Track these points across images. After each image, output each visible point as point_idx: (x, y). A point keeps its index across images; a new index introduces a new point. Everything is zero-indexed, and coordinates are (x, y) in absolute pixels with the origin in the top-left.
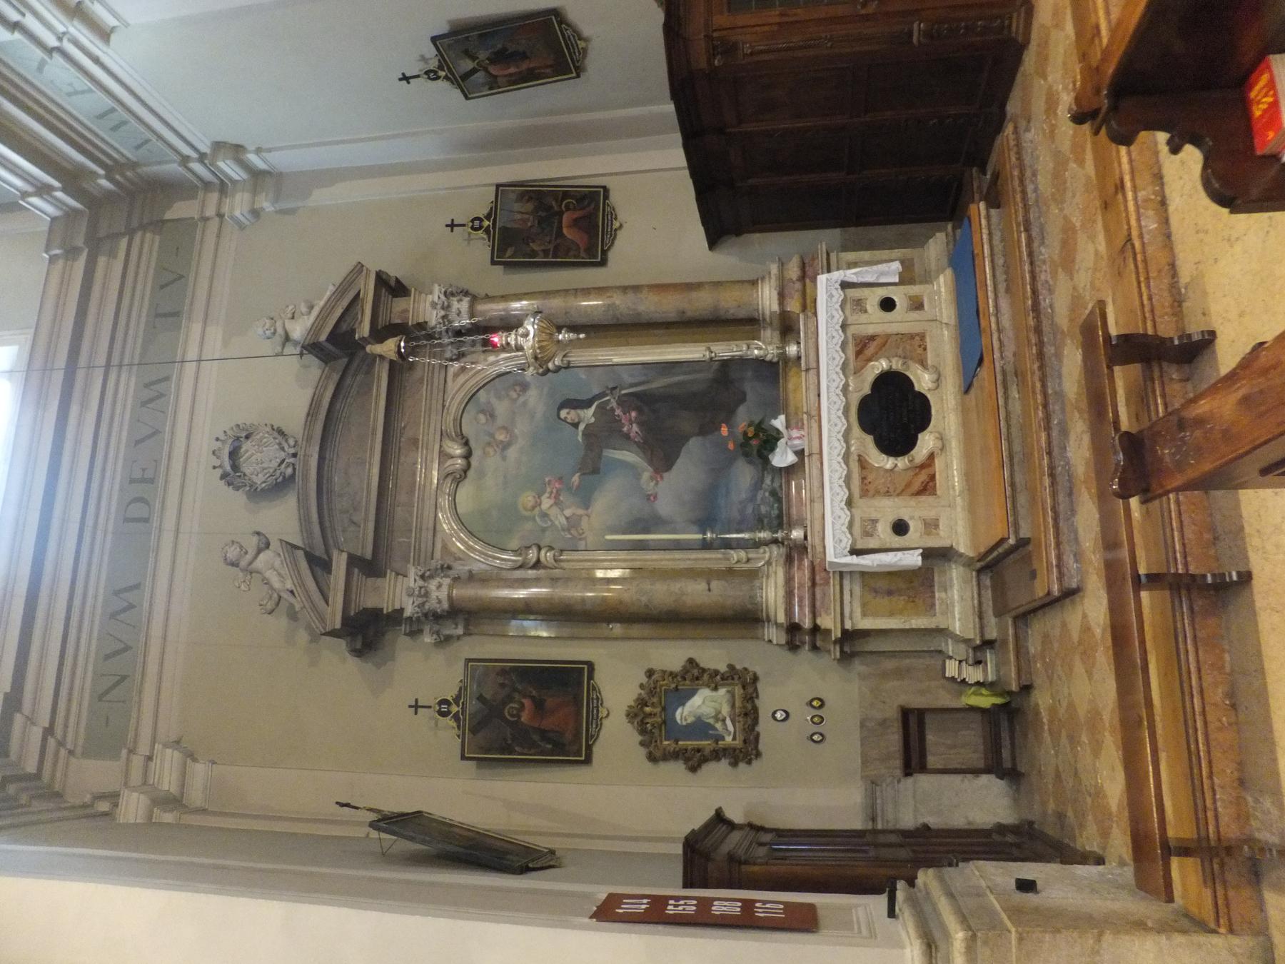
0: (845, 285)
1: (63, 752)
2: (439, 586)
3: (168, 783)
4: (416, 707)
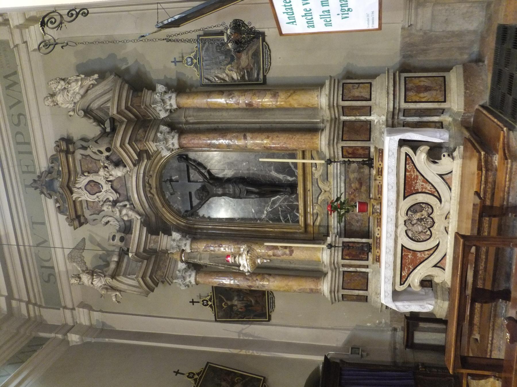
0: (402, 143)
1: (31, 307)
4: (193, 302)
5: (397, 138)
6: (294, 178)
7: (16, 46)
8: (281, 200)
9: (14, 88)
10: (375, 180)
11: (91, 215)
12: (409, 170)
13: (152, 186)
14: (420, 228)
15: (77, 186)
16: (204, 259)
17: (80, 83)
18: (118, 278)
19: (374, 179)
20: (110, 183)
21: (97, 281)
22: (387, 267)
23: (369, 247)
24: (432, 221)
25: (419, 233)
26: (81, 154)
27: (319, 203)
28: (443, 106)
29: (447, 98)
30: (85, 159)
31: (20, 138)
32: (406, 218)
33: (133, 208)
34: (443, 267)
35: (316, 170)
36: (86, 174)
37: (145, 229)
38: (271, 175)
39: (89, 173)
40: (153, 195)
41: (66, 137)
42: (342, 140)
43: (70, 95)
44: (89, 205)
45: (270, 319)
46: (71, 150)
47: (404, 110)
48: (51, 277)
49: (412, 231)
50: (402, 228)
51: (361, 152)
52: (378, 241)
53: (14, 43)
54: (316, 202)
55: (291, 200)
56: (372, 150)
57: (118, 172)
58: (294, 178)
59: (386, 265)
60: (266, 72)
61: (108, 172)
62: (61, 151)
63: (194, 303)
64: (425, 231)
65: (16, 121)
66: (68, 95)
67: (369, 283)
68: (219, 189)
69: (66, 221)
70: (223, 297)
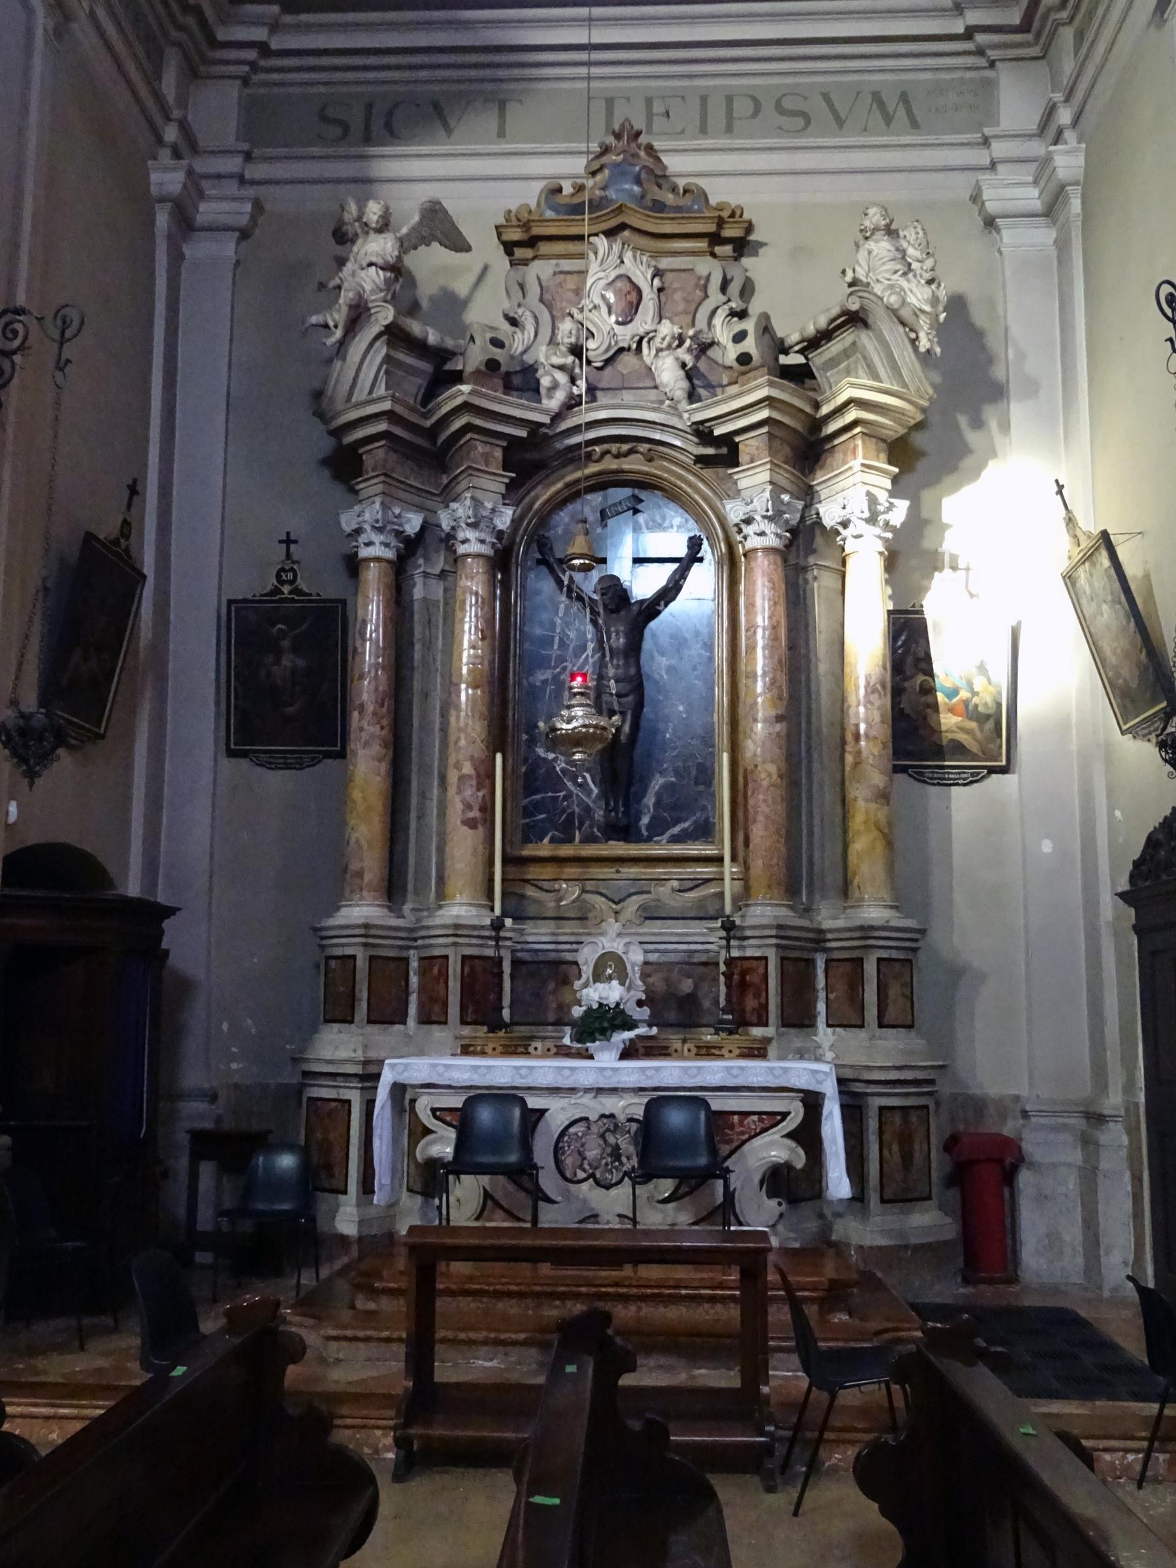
0: (812, 1102)
2: (762, 534)
3: (207, 212)
4: (288, 541)
5: (829, 1088)
6: (645, 833)
7: (986, 142)
8: (586, 799)
9: (877, 115)
10: (684, 1041)
11: (539, 279)
12: (746, 1122)
13: (623, 459)
14: (592, 1153)
15: (628, 256)
16: (425, 584)
17: (927, 308)
18: (385, 337)
19: (688, 1036)
20: (634, 346)
21: (378, 282)
22: (817, 1076)
23: (495, 1025)
24: (614, 1181)
25: (580, 1153)
26: (709, 275)
27: (585, 896)
28: (874, 1198)
29: (888, 1206)
30: (697, 286)
31: (743, 107)
32: (622, 1118)
33: (572, 403)
34: (486, 1213)
35: (673, 890)
36: (657, 282)
37: (523, 433)
38: (653, 776)
39: (660, 290)
40: (597, 461)
41: (753, 237)
42: (783, 959)
43: (895, 277)
44: (569, 277)
45: (231, 754)
46: (718, 250)
47: (860, 1107)
48: (338, 131)
49: (585, 1134)
50: (593, 1107)
51: (751, 1003)
52: (521, 1049)
53: (996, 137)
54: (588, 888)
55: (587, 823)
56: (757, 1032)
57: (668, 373)
58: (645, 833)
59: (610, 1073)
60: (916, 773)
61: (669, 347)
62: (721, 222)
63: (284, 545)
64: (587, 1167)
65: (787, 104)
66: (896, 272)
67: (378, 1026)
68: (622, 640)
69: (521, 206)
70: (304, 627)
